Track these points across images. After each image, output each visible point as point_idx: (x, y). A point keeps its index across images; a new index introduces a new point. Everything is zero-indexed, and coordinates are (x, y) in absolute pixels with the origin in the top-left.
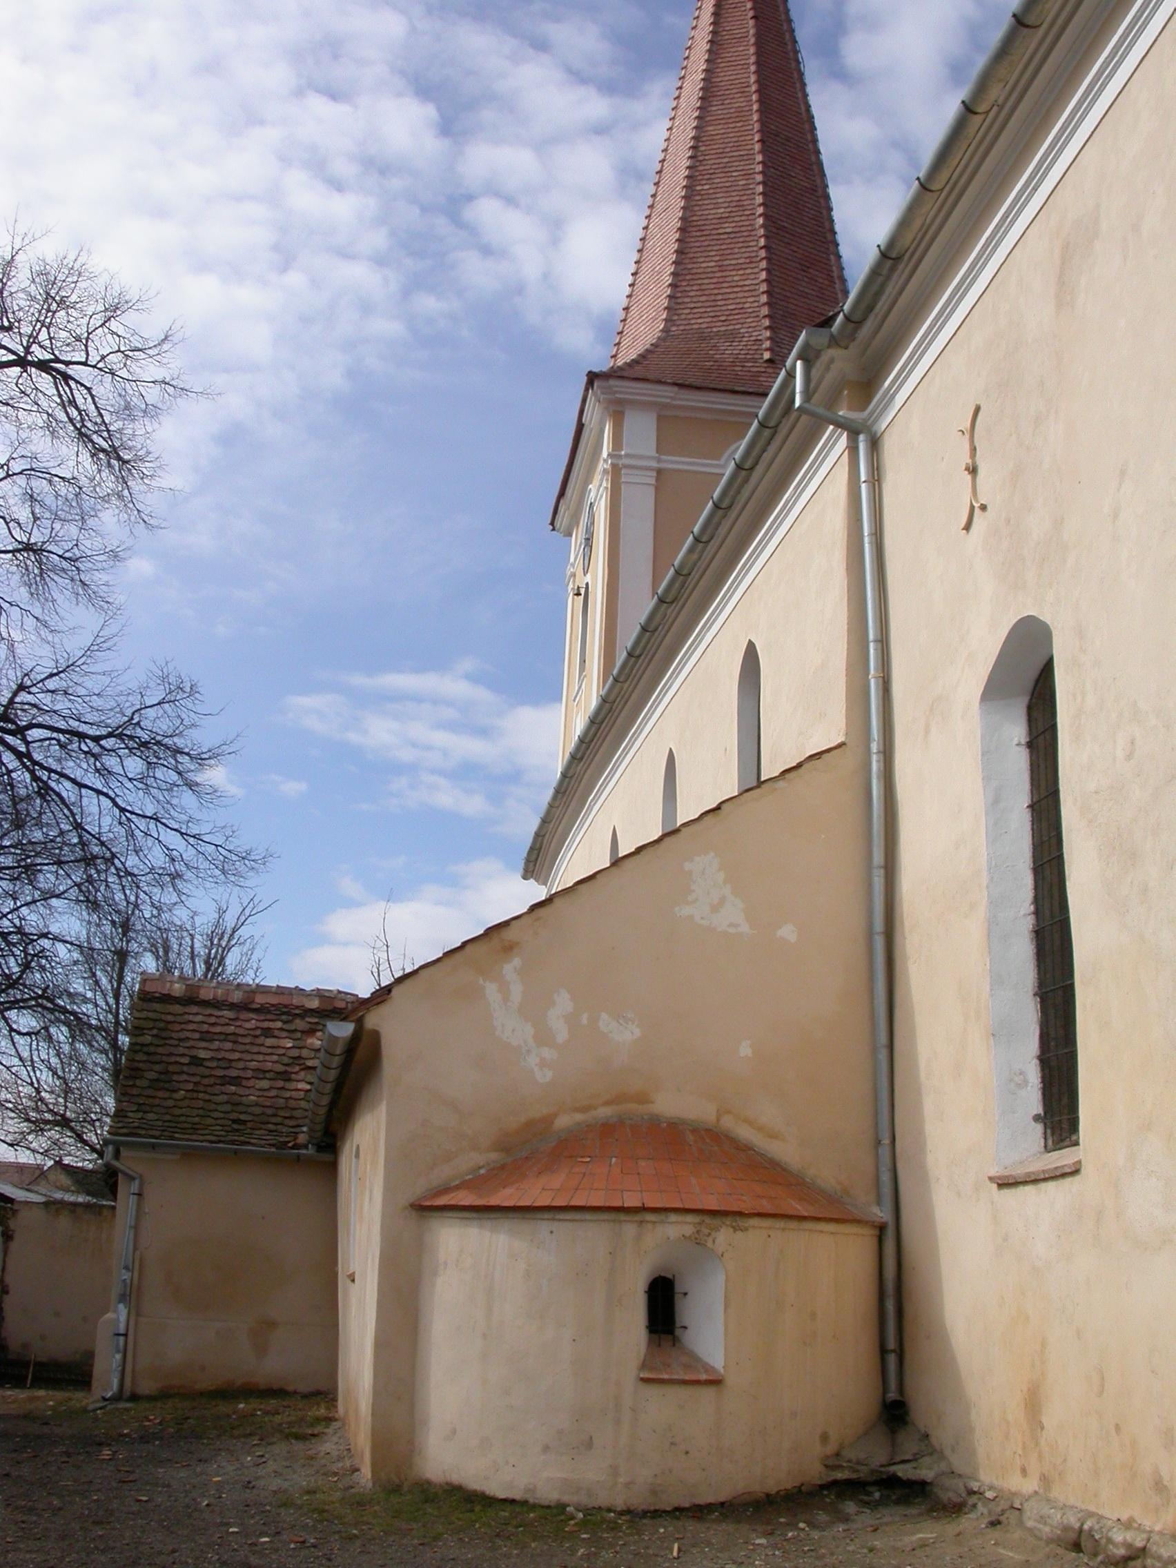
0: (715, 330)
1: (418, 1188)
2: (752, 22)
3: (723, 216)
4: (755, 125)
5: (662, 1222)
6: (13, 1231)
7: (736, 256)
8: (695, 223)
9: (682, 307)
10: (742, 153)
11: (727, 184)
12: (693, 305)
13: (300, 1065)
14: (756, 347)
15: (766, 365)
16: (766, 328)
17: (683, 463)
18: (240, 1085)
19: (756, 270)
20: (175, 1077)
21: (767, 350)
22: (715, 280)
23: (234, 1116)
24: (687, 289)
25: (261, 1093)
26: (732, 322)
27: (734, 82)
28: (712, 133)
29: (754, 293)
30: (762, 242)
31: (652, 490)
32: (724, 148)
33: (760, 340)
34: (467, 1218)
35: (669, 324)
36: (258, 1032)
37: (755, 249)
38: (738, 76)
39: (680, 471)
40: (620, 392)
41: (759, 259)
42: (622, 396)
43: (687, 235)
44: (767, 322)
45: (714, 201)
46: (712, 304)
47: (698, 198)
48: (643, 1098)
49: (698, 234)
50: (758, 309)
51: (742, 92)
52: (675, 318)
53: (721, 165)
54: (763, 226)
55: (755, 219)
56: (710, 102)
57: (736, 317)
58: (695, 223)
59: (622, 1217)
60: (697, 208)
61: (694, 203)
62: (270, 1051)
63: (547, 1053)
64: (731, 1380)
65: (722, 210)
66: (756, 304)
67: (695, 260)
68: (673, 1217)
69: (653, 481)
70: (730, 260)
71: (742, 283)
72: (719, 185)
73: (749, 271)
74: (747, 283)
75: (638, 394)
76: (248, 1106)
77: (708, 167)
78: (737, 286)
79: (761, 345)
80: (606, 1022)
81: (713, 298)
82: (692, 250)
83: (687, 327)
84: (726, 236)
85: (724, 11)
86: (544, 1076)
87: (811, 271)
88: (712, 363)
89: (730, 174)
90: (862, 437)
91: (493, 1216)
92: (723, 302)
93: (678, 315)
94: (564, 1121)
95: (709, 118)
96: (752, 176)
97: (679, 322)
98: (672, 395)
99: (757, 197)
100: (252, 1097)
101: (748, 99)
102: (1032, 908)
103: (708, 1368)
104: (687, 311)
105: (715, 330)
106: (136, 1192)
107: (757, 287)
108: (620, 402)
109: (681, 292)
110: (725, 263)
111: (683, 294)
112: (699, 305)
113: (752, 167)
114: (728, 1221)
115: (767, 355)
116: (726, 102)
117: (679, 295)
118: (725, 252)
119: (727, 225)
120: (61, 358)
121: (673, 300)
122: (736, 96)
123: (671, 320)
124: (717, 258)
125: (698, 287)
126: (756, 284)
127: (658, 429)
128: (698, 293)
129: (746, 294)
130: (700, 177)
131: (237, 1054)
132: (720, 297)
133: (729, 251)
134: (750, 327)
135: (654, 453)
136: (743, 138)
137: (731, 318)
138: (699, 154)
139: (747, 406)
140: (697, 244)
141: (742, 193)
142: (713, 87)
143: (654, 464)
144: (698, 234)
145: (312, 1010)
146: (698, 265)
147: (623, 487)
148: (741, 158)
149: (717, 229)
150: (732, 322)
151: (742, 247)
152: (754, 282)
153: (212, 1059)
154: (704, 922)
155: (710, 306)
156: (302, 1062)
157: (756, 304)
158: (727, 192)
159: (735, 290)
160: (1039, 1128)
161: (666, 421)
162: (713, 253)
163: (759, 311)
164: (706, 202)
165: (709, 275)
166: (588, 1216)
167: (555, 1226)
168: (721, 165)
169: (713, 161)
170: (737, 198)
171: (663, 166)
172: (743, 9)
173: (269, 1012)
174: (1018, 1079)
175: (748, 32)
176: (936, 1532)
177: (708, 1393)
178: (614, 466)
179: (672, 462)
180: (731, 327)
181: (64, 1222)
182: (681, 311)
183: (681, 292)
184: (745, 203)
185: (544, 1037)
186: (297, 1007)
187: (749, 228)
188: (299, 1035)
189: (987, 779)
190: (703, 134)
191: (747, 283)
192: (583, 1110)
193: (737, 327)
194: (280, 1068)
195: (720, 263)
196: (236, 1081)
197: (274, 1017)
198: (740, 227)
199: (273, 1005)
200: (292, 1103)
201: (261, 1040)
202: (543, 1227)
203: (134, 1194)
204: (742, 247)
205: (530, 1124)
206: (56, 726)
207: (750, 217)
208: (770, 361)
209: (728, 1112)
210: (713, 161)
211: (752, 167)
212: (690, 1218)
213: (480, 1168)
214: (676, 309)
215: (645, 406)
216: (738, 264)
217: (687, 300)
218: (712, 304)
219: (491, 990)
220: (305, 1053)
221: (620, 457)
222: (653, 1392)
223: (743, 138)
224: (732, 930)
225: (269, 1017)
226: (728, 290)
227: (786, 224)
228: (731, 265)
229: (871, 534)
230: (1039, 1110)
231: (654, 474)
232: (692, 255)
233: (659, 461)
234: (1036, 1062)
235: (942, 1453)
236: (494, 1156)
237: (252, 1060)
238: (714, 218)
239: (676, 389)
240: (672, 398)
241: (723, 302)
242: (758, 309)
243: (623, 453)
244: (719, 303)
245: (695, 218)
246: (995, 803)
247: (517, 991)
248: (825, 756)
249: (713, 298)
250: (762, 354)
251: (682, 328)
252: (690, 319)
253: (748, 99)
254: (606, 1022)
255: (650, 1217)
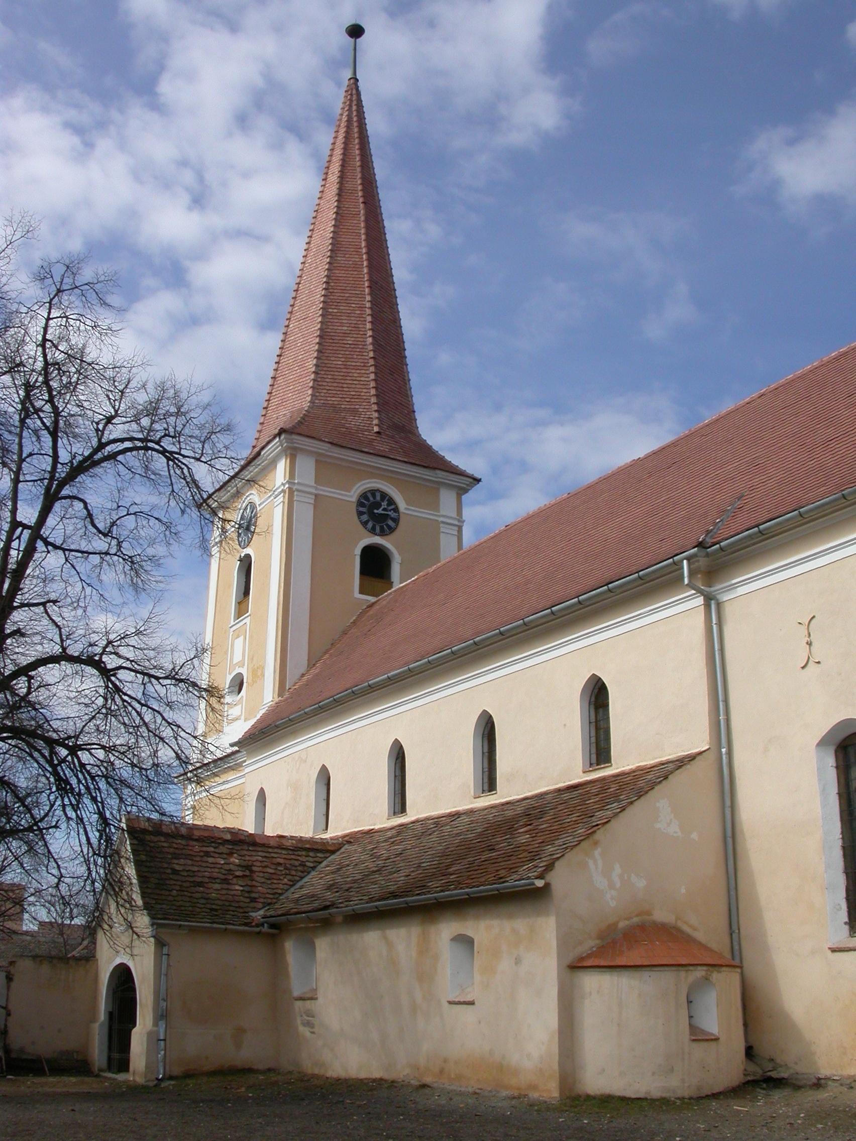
0: (343, 406)
1: (570, 958)
2: (362, 206)
3: (346, 332)
4: (366, 275)
5: (695, 970)
6: (13, 975)
7: (355, 360)
8: (328, 334)
9: (322, 388)
10: (357, 292)
11: (348, 312)
12: (328, 388)
13: (232, 875)
14: (369, 422)
15: (376, 435)
16: (376, 411)
17: (327, 491)
18: (203, 887)
19: (367, 372)
20: (168, 882)
21: (376, 425)
22: (342, 374)
23: (209, 906)
24: (325, 376)
25: (217, 892)
26: (353, 403)
27: (351, 243)
28: (338, 275)
29: (366, 386)
30: (371, 354)
31: (312, 507)
32: (346, 287)
33: (372, 418)
34: (661, 971)
35: (314, 398)
36: (202, 854)
37: (367, 357)
38: (355, 240)
39: (327, 496)
40: (298, 443)
41: (369, 365)
42: (297, 446)
43: (323, 341)
44: (375, 407)
45: (340, 321)
46: (341, 389)
47: (330, 317)
48: (649, 913)
49: (331, 341)
50: (369, 398)
51: (357, 252)
52: (317, 394)
53: (344, 298)
54: (372, 344)
55: (367, 338)
56: (336, 254)
57: (356, 400)
58: (328, 334)
59: (680, 968)
60: (330, 324)
61: (328, 320)
62: (212, 866)
63: (614, 893)
64: (723, 1039)
65: (346, 328)
66: (368, 394)
67: (329, 358)
68: (699, 968)
69: (312, 501)
70: (352, 362)
71: (359, 379)
72: (343, 311)
73: (364, 372)
74: (362, 379)
75: (308, 446)
76: (213, 900)
77: (336, 297)
78: (356, 380)
79: (372, 421)
80: (634, 878)
81: (341, 385)
82: (327, 351)
83: (325, 402)
84: (348, 346)
85: (344, 194)
86: (613, 904)
87: (395, 375)
88: (344, 430)
89: (350, 305)
90: (713, 602)
91: (618, 970)
92: (347, 389)
93: (320, 393)
94: (621, 925)
95: (335, 265)
96: (364, 309)
97: (320, 398)
98: (327, 448)
99: (368, 324)
100: (213, 895)
101: (360, 257)
102: (841, 836)
103: (712, 1034)
104: (325, 391)
105: (343, 406)
106: (166, 953)
107: (369, 383)
108: (295, 449)
109: (321, 378)
110: (349, 363)
111: (323, 379)
112: (333, 388)
113: (364, 303)
114: (717, 968)
115: (376, 429)
116: (347, 256)
117: (319, 379)
118: (348, 356)
119: (348, 339)
120: (168, 449)
121: (316, 383)
122: (353, 253)
123: (315, 396)
124: (343, 360)
125: (332, 377)
126: (368, 381)
127: (316, 469)
128: (331, 380)
129: (362, 387)
130: (331, 304)
131: (195, 867)
132: (345, 386)
133: (350, 356)
134: (364, 408)
135: (313, 484)
136: (357, 283)
137: (353, 400)
138: (330, 287)
139: (368, 461)
140: (331, 348)
141: (358, 319)
142: (338, 244)
143: (313, 491)
144: (331, 341)
145: (228, 841)
146: (331, 362)
147: (295, 503)
148: (357, 295)
149: (343, 340)
150: (353, 403)
151: (359, 355)
152: (367, 379)
153: (184, 870)
154: (665, 831)
155: (339, 391)
156: (232, 873)
157: (368, 394)
158: (348, 316)
159: (355, 382)
160: (847, 927)
161: (321, 463)
162: (341, 356)
163: (370, 399)
164: (335, 321)
165: (339, 370)
166: (666, 968)
167: (652, 973)
168: (344, 298)
169: (339, 294)
170: (355, 322)
171: (298, 287)
172: (356, 195)
173: (204, 841)
174: (838, 907)
175: (360, 211)
176: (564, 1118)
177: (713, 1044)
178: (290, 488)
179: (324, 491)
180: (352, 407)
181: (45, 969)
182: (321, 391)
183: (321, 378)
184: (360, 326)
185: (611, 886)
186: (219, 839)
187: (363, 343)
188: (225, 856)
189: (820, 780)
190: (332, 275)
191: (362, 379)
192: (628, 919)
193: (357, 407)
194: (223, 877)
195: (345, 363)
196: (201, 884)
197: (207, 845)
198: (357, 341)
199: (205, 837)
200: (237, 898)
201: (205, 859)
202: (646, 974)
203: (165, 954)
204: (359, 355)
205: (609, 926)
206: (156, 675)
207: (363, 336)
208: (378, 433)
209: (680, 919)
210: (339, 294)
211: (364, 303)
212: (705, 968)
213: (593, 947)
214: (318, 389)
215: (309, 453)
216: (356, 365)
217: (324, 384)
218: (341, 389)
219: (591, 863)
220: (232, 867)
221: (294, 483)
222: (695, 1045)
223: (357, 283)
224: (675, 835)
225: (205, 844)
226: (350, 382)
227: (382, 343)
228: (352, 365)
229: (718, 650)
230: (847, 920)
231: (314, 497)
232: (326, 355)
233: (316, 489)
234: (844, 900)
235: (786, 1065)
236: (598, 942)
237: (205, 872)
238: (340, 333)
239: (329, 445)
240: (326, 451)
241: (347, 389)
242: (369, 398)
243: (296, 481)
244: (345, 389)
245: (329, 330)
246: (823, 791)
247: (600, 862)
248: (704, 753)
249: (341, 385)
250: (373, 427)
251: (322, 402)
252: (327, 397)
253: (360, 257)
254: (634, 878)
255: (691, 968)
